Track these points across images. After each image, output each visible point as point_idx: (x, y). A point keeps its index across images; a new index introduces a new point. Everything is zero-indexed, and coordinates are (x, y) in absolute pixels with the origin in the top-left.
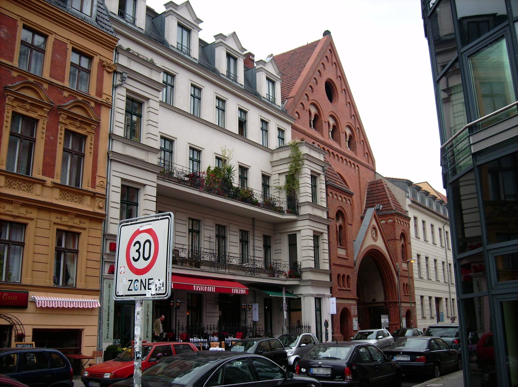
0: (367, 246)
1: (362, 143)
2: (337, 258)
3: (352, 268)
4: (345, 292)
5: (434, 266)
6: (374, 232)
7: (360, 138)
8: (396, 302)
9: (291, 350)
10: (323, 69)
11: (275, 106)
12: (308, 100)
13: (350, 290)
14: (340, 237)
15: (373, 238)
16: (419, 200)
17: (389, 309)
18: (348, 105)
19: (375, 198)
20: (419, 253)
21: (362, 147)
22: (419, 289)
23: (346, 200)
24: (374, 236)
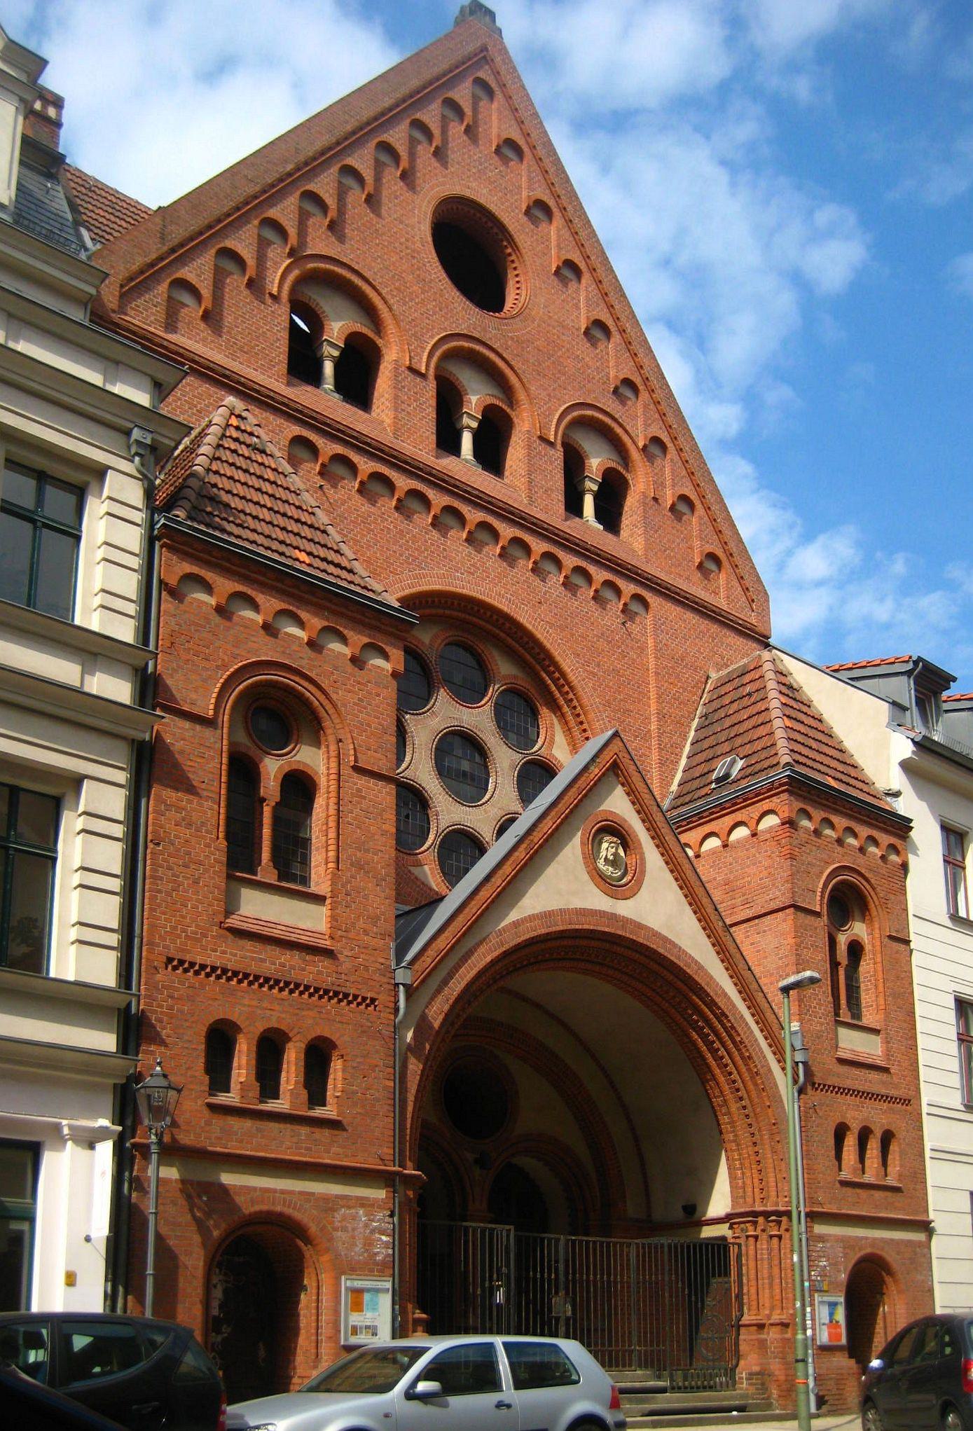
22: (950, 1156)
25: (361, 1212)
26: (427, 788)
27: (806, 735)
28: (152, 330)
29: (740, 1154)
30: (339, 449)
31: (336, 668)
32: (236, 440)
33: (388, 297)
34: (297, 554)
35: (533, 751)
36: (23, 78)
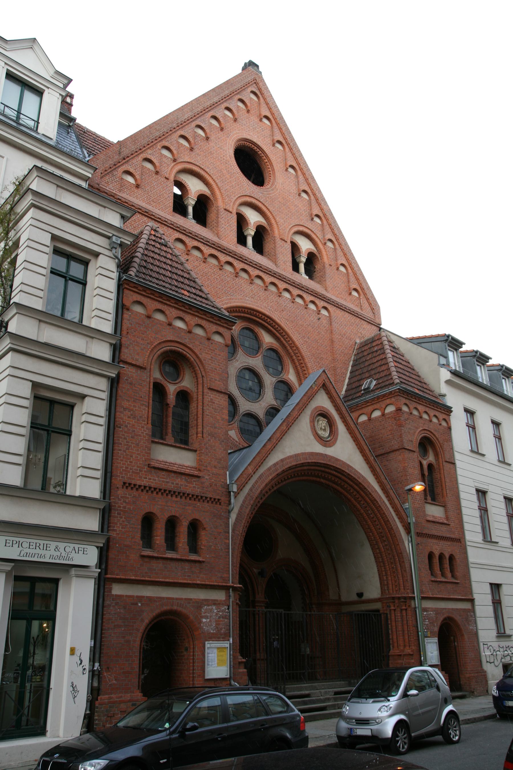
3: (218, 501)
4: (173, 564)
8: (405, 598)
9: (387, 704)
22: (482, 566)
23: (419, 413)
25: (214, 608)
26: (234, 394)
27: (404, 369)
28: (114, 192)
29: (385, 568)
30: (196, 243)
31: (201, 343)
32: (154, 241)
33: (216, 180)
34: (183, 292)
35: (280, 376)
36: (62, 86)
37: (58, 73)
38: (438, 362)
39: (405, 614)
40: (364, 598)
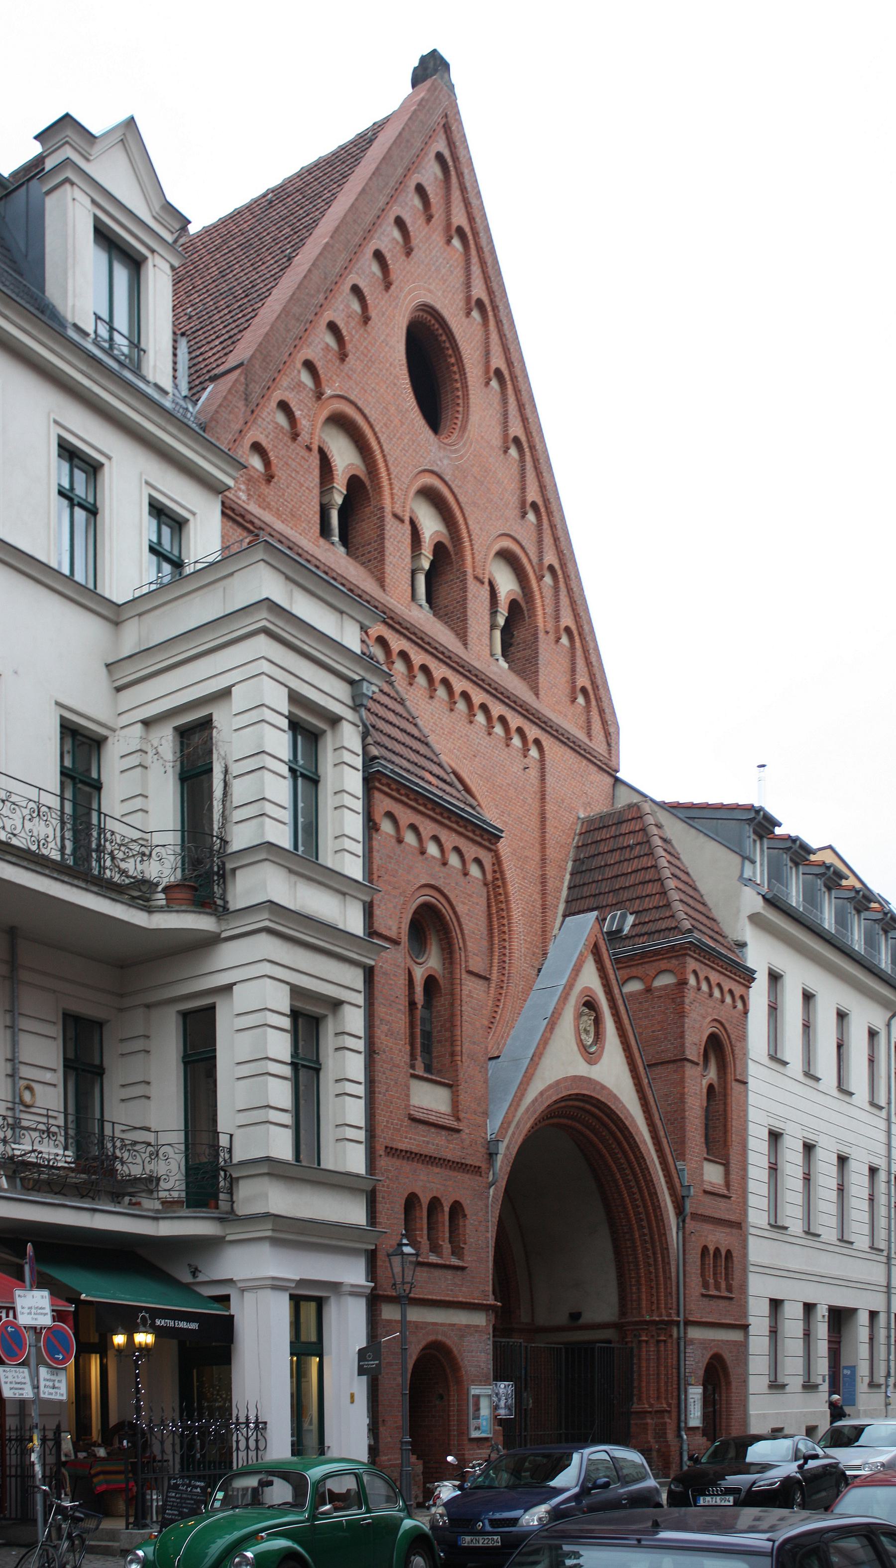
0: (549, 1082)
1: (565, 640)
2: (407, 1122)
3: (476, 1170)
4: (437, 1273)
5: (833, 1184)
6: (587, 1022)
7: (557, 618)
10: (399, 250)
11: (142, 385)
12: (319, 395)
13: (463, 1268)
14: (427, 1035)
15: (584, 1049)
16: (795, 898)
17: (635, 1351)
18: (513, 452)
19: (605, 887)
20: (778, 1125)
21: (565, 663)
24: (589, 1040)
37: (170, 209)
38: (738, 874)
39: (662, 1349)
40: (582, 1321)
